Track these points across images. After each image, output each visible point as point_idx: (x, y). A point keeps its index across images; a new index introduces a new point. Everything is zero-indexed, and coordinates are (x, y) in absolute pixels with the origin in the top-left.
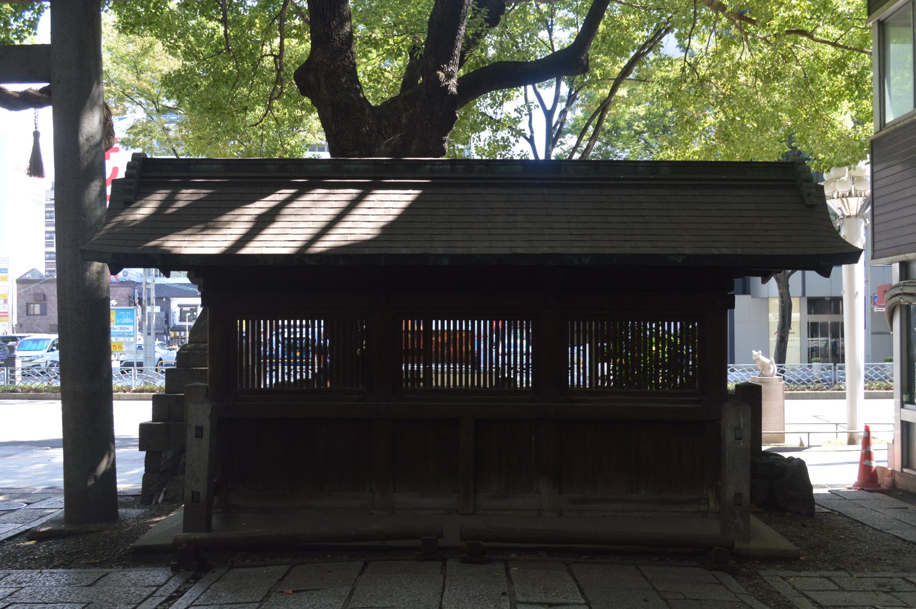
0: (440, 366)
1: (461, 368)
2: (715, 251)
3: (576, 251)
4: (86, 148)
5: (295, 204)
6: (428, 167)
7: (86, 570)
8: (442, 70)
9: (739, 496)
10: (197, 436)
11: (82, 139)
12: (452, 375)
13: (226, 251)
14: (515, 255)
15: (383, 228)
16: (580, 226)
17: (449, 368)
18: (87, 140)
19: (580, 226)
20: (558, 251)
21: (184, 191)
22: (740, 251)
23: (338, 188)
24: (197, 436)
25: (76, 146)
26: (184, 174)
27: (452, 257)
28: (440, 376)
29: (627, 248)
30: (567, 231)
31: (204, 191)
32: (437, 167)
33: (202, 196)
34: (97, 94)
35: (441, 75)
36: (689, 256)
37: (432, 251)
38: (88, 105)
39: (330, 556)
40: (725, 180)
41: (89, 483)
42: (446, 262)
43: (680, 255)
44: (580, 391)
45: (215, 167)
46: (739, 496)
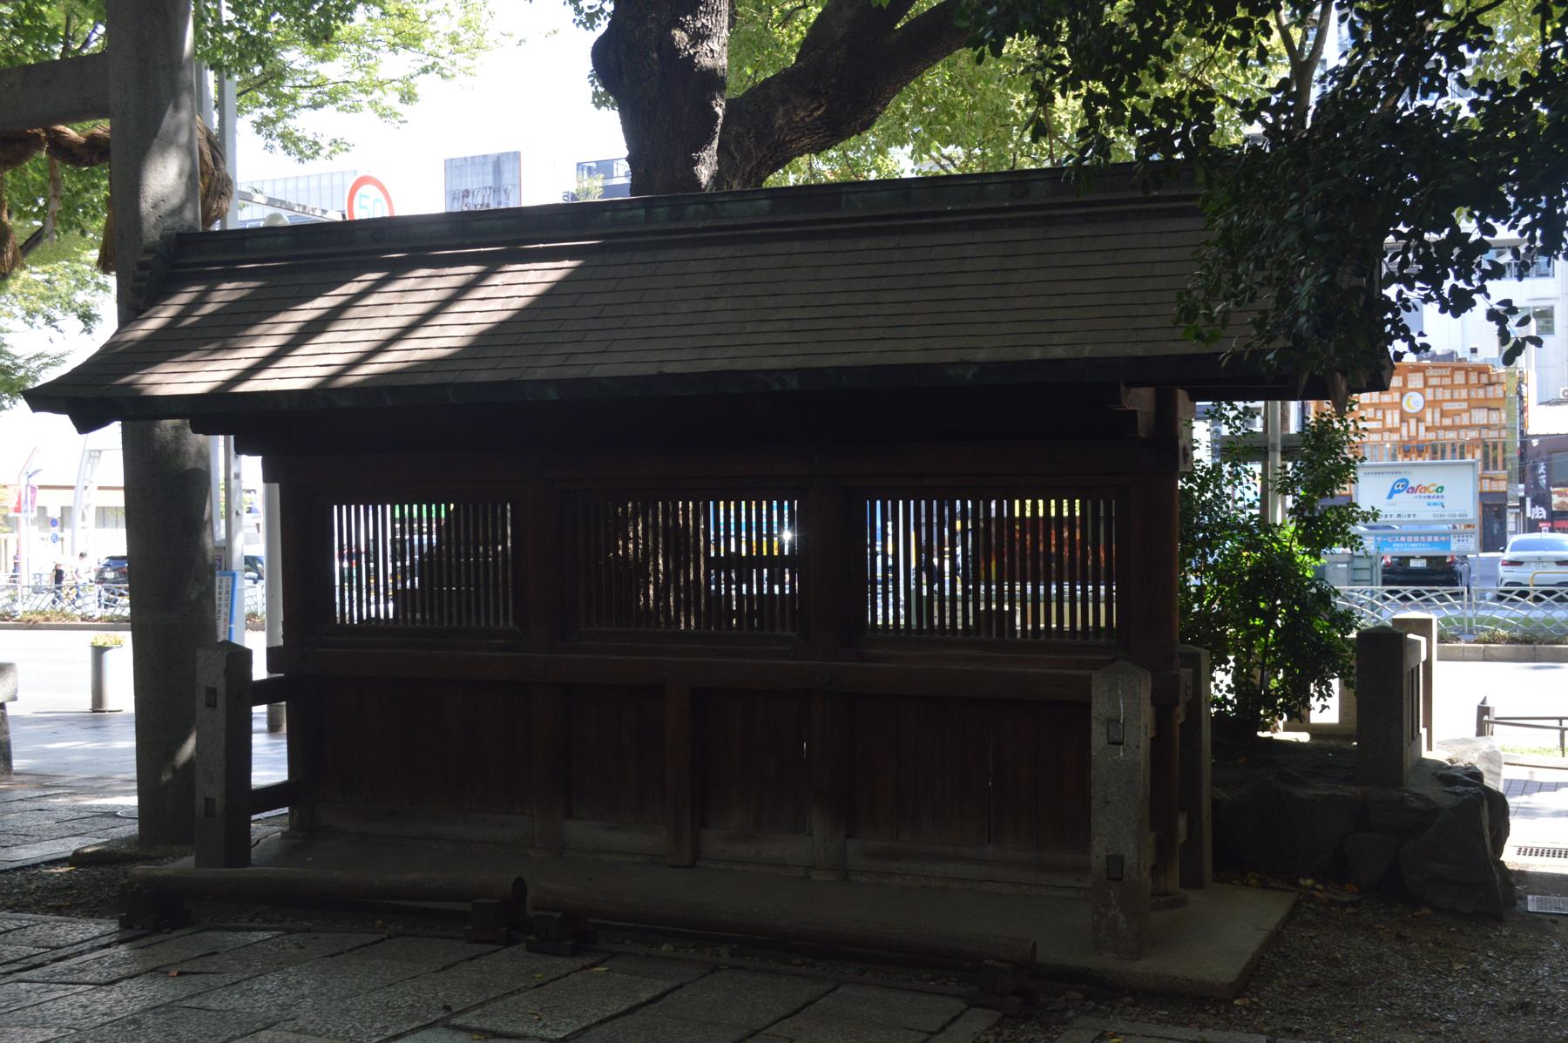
0: (1066, 588)
1: (1084, 591)
2: (1037, 354)
3: (772, 364)
4: (153, 219)
5: (374, 299)
6: (608, 214)
7: (175, 934)
8: (682, 27)
9: (1116, 861)
10: (208, 705)
11: (146, 206)
12: (1066, 605)
13: (364, 381)
14: (661, 375)
15: (481, 335)
16: (806, 313)
17: (1084, 591)
18: (155, 207)
19: (806, 313)
20: (740, 365)
21: (226, 286)
22: (1087, 351)
23: (451, 266)
24: (208, 705)
25: (136, 217)
26: (230, 257)
27: (560, 384)
28: (1054, 606)
29: (871, 355)
30: (786, 326)
31: (567, 263)
32: (623, 215)
33: (245, 292)
34: (172, 127)
35: (680, 36)
36: (982, 365)
37: (528, 376)
38: (155, 148)
39: (379, 922)
40: (787, 224)
41: (164, 779)
42: (552, 394)
43: (965, 364)
44: (891, 635)
45: (280, 240)
46: (1116, 861)
